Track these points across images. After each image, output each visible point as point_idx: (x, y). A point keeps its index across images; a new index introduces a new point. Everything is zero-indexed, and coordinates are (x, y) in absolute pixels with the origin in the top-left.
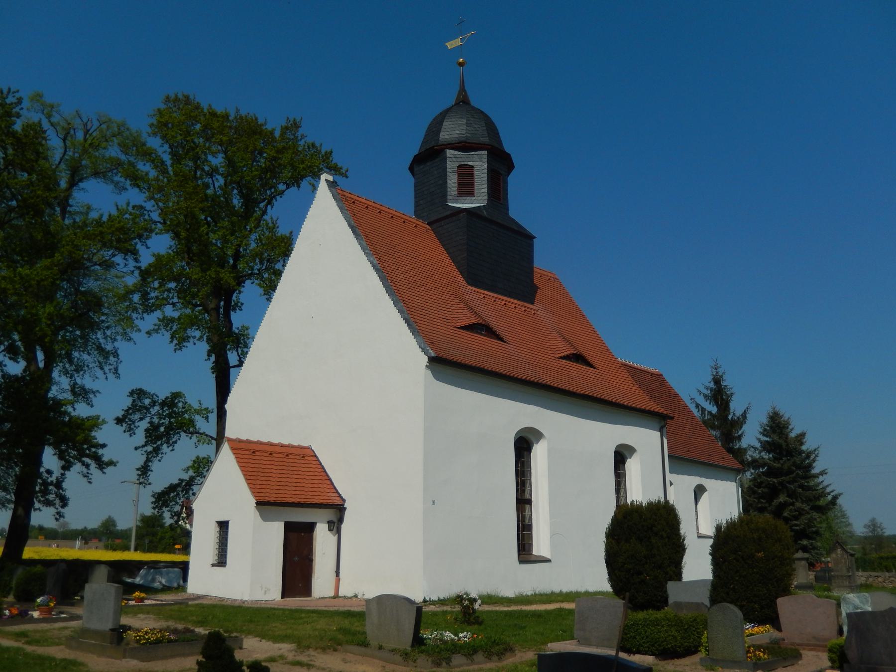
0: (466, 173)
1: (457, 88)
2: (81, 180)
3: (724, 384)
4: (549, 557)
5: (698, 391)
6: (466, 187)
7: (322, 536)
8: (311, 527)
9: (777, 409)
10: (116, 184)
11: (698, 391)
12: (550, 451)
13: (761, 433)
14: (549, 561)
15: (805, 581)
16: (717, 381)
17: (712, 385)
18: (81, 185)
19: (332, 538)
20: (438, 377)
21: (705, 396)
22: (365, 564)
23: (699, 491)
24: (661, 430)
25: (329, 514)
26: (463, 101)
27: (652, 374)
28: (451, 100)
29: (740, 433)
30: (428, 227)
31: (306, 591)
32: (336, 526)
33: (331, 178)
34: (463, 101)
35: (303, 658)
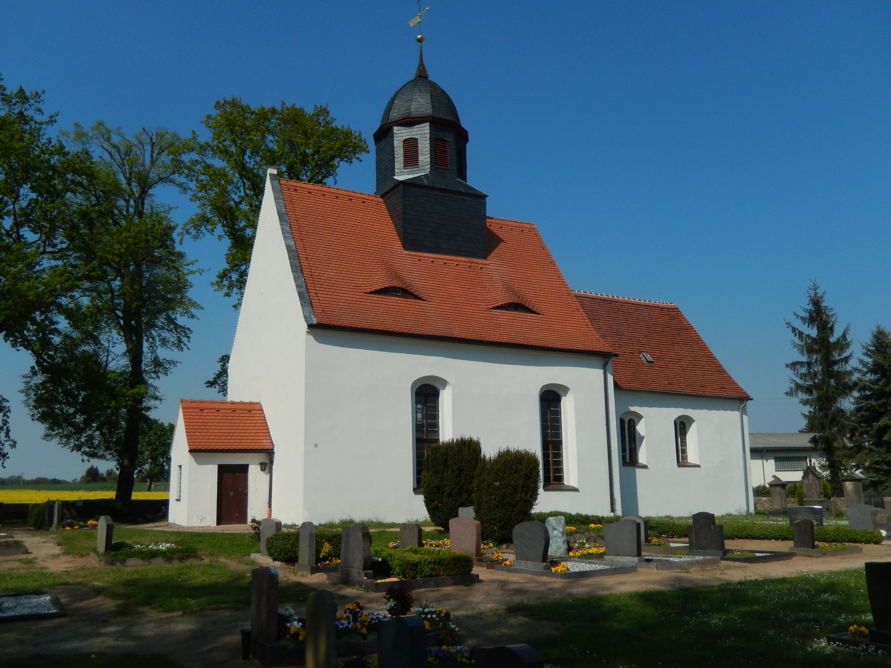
0: (411, 145)
1: (417, 64)
2: (150, 187)
3: (823, 304)
4: (576, 486)
5: (795, 314)
6: (411, 158)
7: (255, 477)
8: (244, 469)
9: (882, 327)
10: (180, 185)
11: (795, 314)
12: (455, 397)
14: (576, 490)
15: (762, 509)
16: (816, 303)
17: (810, 307)
18: (150, 191)
19: (265, 477)
20: (319, 340)
21: (803, 319)
22: (285, 497)
23: (682, 426)
24: (604, 367)
25: (262, 458)
26: (422, 75)
27: (662, 309)
28: (412, 75)
29: (845, 355)
30: (381, 200)
31: (241, 517)
32: (267, 467)
33: (275, 172)
34: (422, 75)
35: (136, 568)
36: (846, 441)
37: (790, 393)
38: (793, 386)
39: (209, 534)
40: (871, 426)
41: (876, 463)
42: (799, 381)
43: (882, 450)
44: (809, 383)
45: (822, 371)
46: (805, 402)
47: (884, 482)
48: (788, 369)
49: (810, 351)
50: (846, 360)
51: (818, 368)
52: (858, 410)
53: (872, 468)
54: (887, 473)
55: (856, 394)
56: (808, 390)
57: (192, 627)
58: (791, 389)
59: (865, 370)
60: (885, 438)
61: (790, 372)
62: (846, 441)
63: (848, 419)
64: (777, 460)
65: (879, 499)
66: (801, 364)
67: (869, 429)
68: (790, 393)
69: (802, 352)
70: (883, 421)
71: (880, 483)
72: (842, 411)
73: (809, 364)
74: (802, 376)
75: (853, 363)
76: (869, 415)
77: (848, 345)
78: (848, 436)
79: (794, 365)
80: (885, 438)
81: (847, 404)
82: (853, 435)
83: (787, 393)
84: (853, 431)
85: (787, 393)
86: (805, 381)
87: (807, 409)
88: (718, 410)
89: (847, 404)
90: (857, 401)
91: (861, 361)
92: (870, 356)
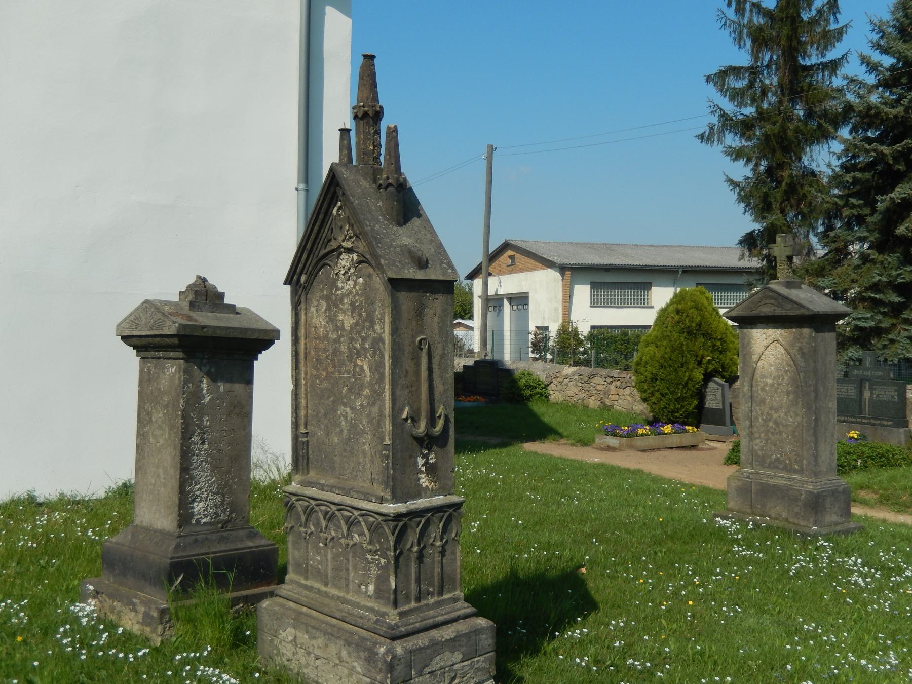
13: (877, 46)
29: (832, 55)
36: (814, 240)
37: (706, 138)
38: (715, 119)
39: (214, 339)
40: (872, 204)
41: (875, 287)
42: (729, 107)
43: (892, 259)
44: (750, 111)
45: (781, 85)
46: (737, 154)
47: (887, 331)
48: (711, 85)
49: (760, 40)
50: (833, 66)
51: (772, 80)
52: (846, 168)
53: (863, 299)
54: (896, 310)
55: (845, 132)
56: (745, 127)
57: (897, 231)
58: (712, 129)
59: (871, 80)
60: (901, 230)
61: (712, 92)
62: (814, 240)
63: (822, 190)
64: (594, 286)
65: (888, 394)
66: (735, 71)
67: (867, 211)
68: (706, 138)
69: (739, 40)
70: (900, 192)
71: (878, 332)
72: (813, 174)
73: (754, 71)
74: (736, 96)
75: (854, 69)
76: (868, 180)
77: (840, 34)
78: (821, 229)
79: (721, 78)
80: (901, 230)
81: (824, 158)
82: (829, 228)
83: (701, 137)
84: (831, 215)
85: (701, 137)
86: (739, 105)
87: (742, 171)
88: (351, 83)
89: (824, 158)
90: (851, 150)
91: (865, 60)
92: (885, 51)
